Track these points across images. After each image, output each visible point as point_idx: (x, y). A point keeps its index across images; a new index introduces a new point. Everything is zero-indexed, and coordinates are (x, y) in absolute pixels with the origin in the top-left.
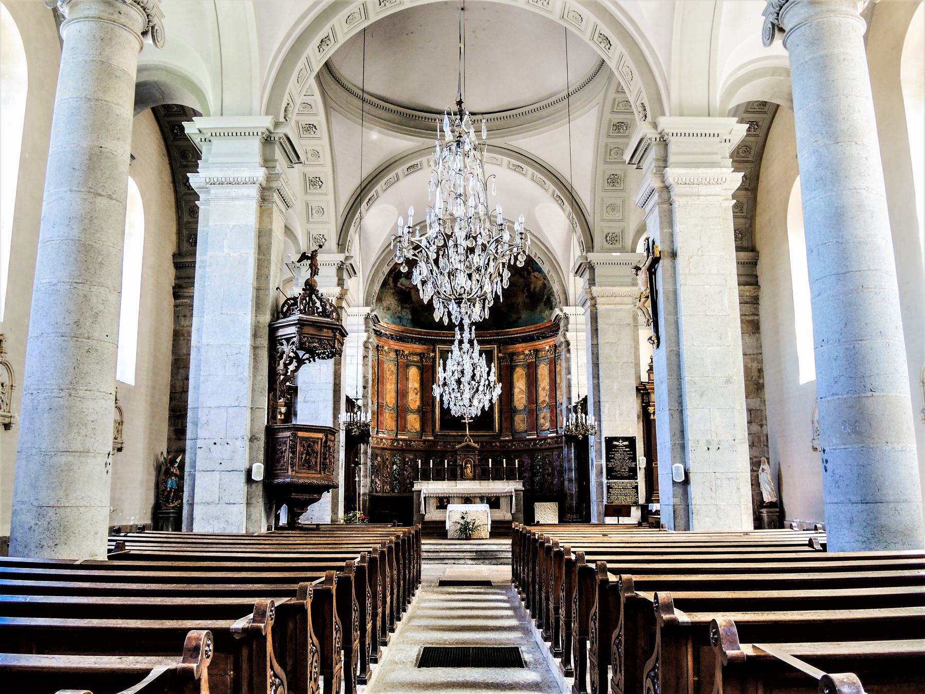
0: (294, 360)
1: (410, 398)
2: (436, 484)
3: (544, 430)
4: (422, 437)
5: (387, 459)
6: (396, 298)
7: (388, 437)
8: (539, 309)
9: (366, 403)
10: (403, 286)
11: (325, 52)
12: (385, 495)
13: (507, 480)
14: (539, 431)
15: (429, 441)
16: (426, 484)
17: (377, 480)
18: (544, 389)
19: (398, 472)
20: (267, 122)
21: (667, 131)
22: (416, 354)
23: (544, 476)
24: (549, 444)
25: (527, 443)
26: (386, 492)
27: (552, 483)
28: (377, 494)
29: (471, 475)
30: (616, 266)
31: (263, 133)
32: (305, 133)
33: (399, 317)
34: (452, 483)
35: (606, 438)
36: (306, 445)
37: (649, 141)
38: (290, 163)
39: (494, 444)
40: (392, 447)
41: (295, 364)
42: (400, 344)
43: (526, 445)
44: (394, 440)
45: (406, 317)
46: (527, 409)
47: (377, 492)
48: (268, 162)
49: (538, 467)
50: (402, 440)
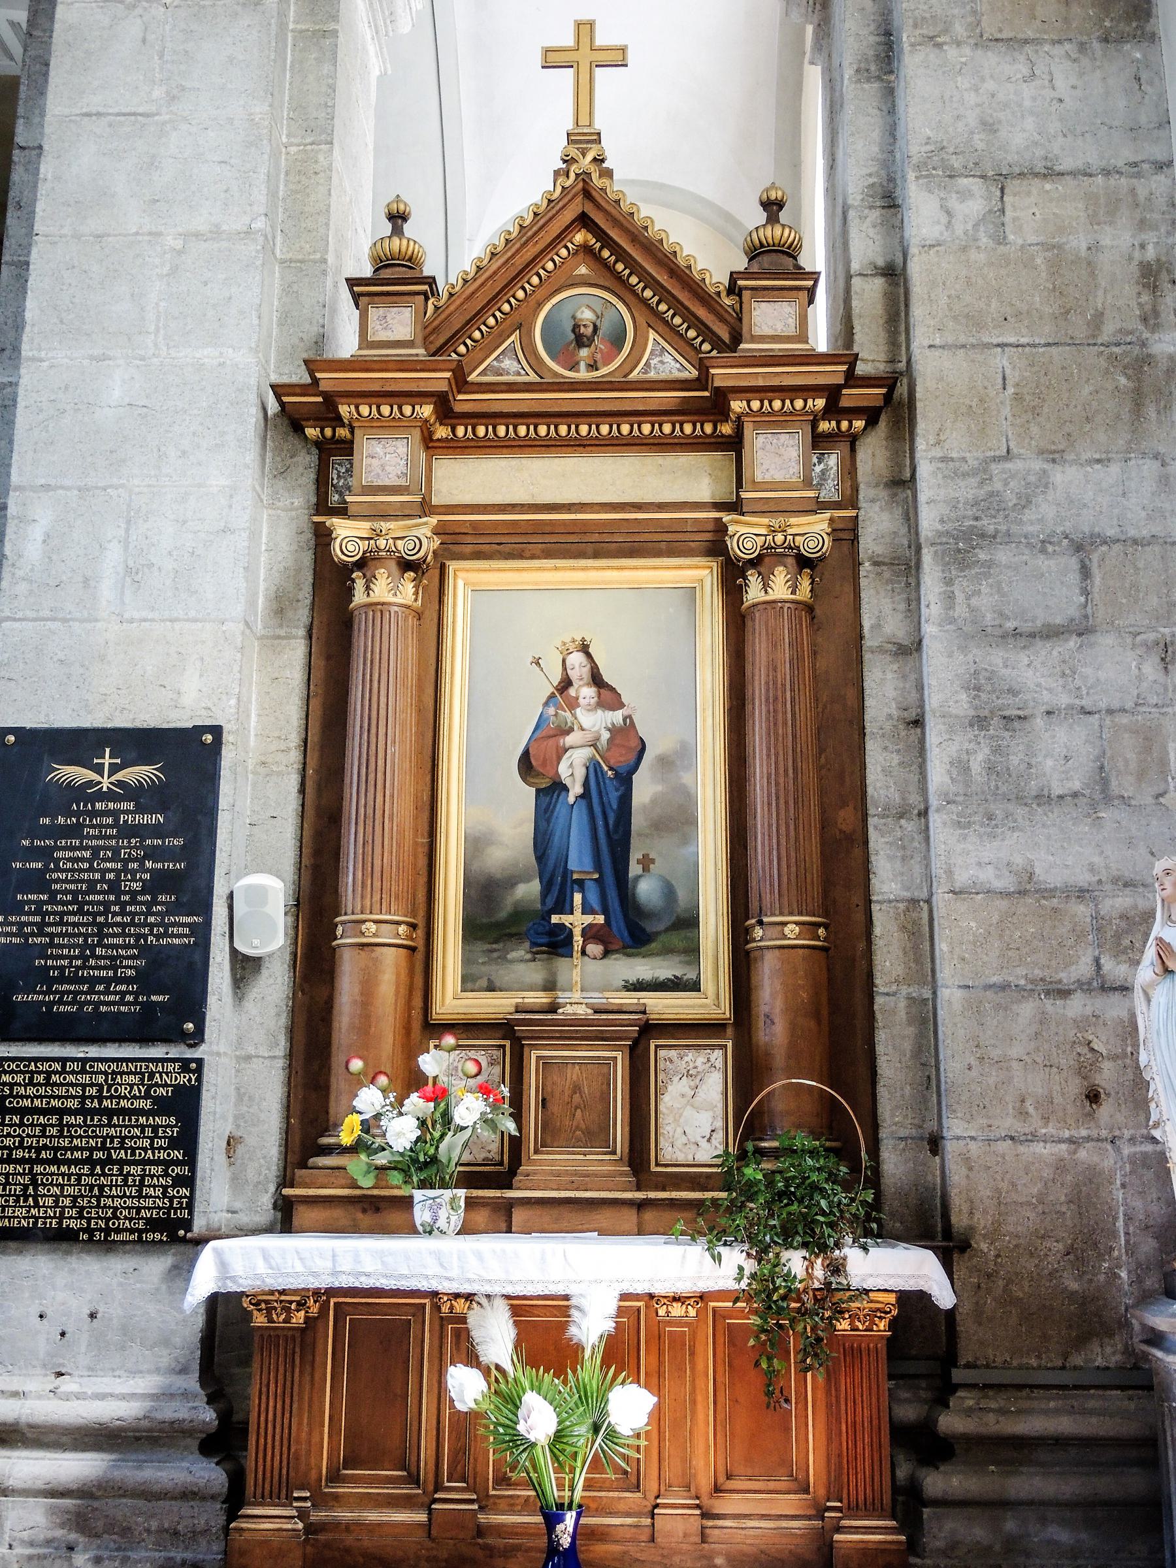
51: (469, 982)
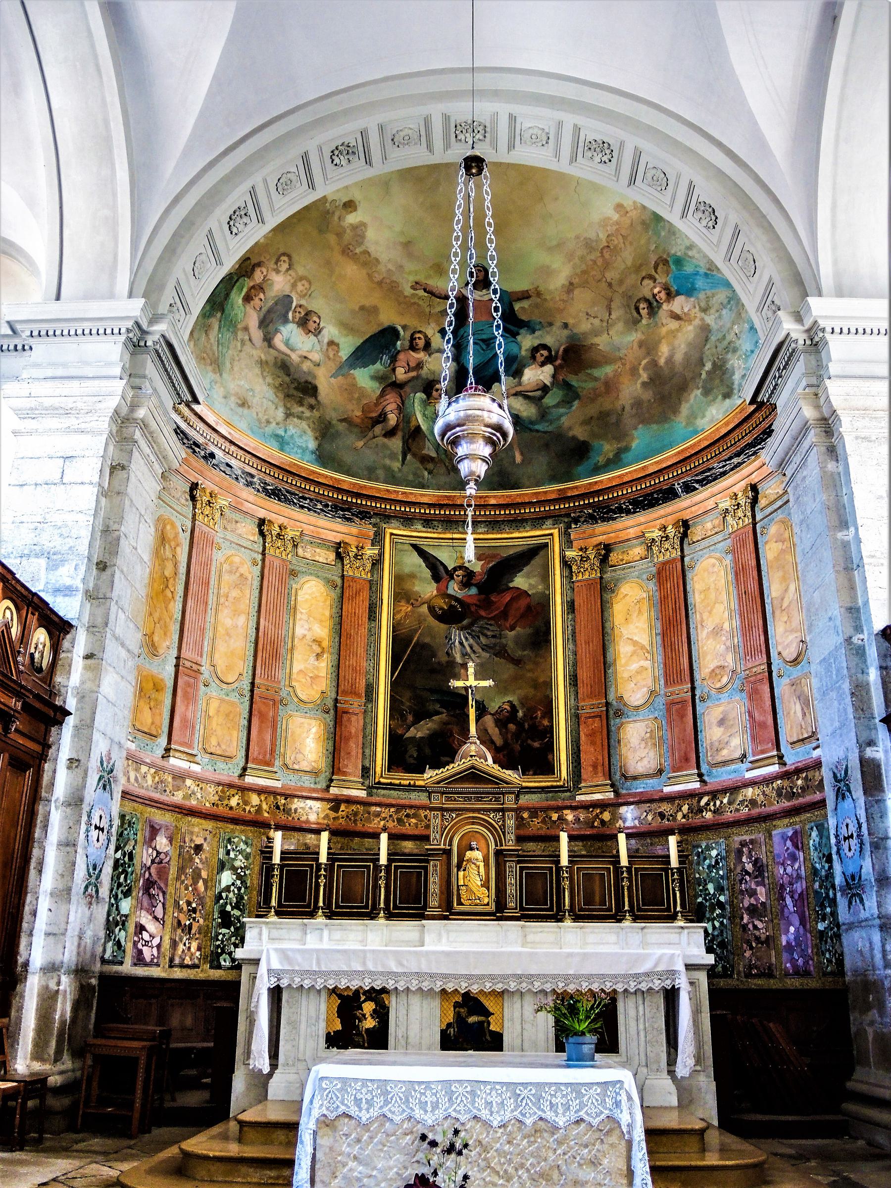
1: (297, 667)
2: (337, 935)
3: (725, 763)
4: (328, 787)
5: (198, 848)
6: (269, 379)
7: (210, 775)
8: (685, 409)
9: (99, 621)
10: (292, 350)
12: (178, 974)
13: (636, 919)
14: (704, 768)
15: (349, 801)
16: (297, 934)
17: (145, 919)
18: (717, 631)
19: (240, 897)
20: (135, 308)
21: (822, 323)
22: (323, 543)
23: (735, 916)
24: (753, 803)
25: (665, 807)
26: (182, 966)
27: (770, 942)
28: (141, 971)
29: (486, 897)
30: (874, 336)
31: (128, 331)
33: (277, 437)
34: (406, 929)
37: (793, 345)
39: (555, 817)
40: (221, 810)
42: (274, 504)
43: (662, 815)
44: (230, 786)
45: (300, 442)
46: (661, 701)
47: (139, 960)
49: (711, 888)
50: (261, 791)
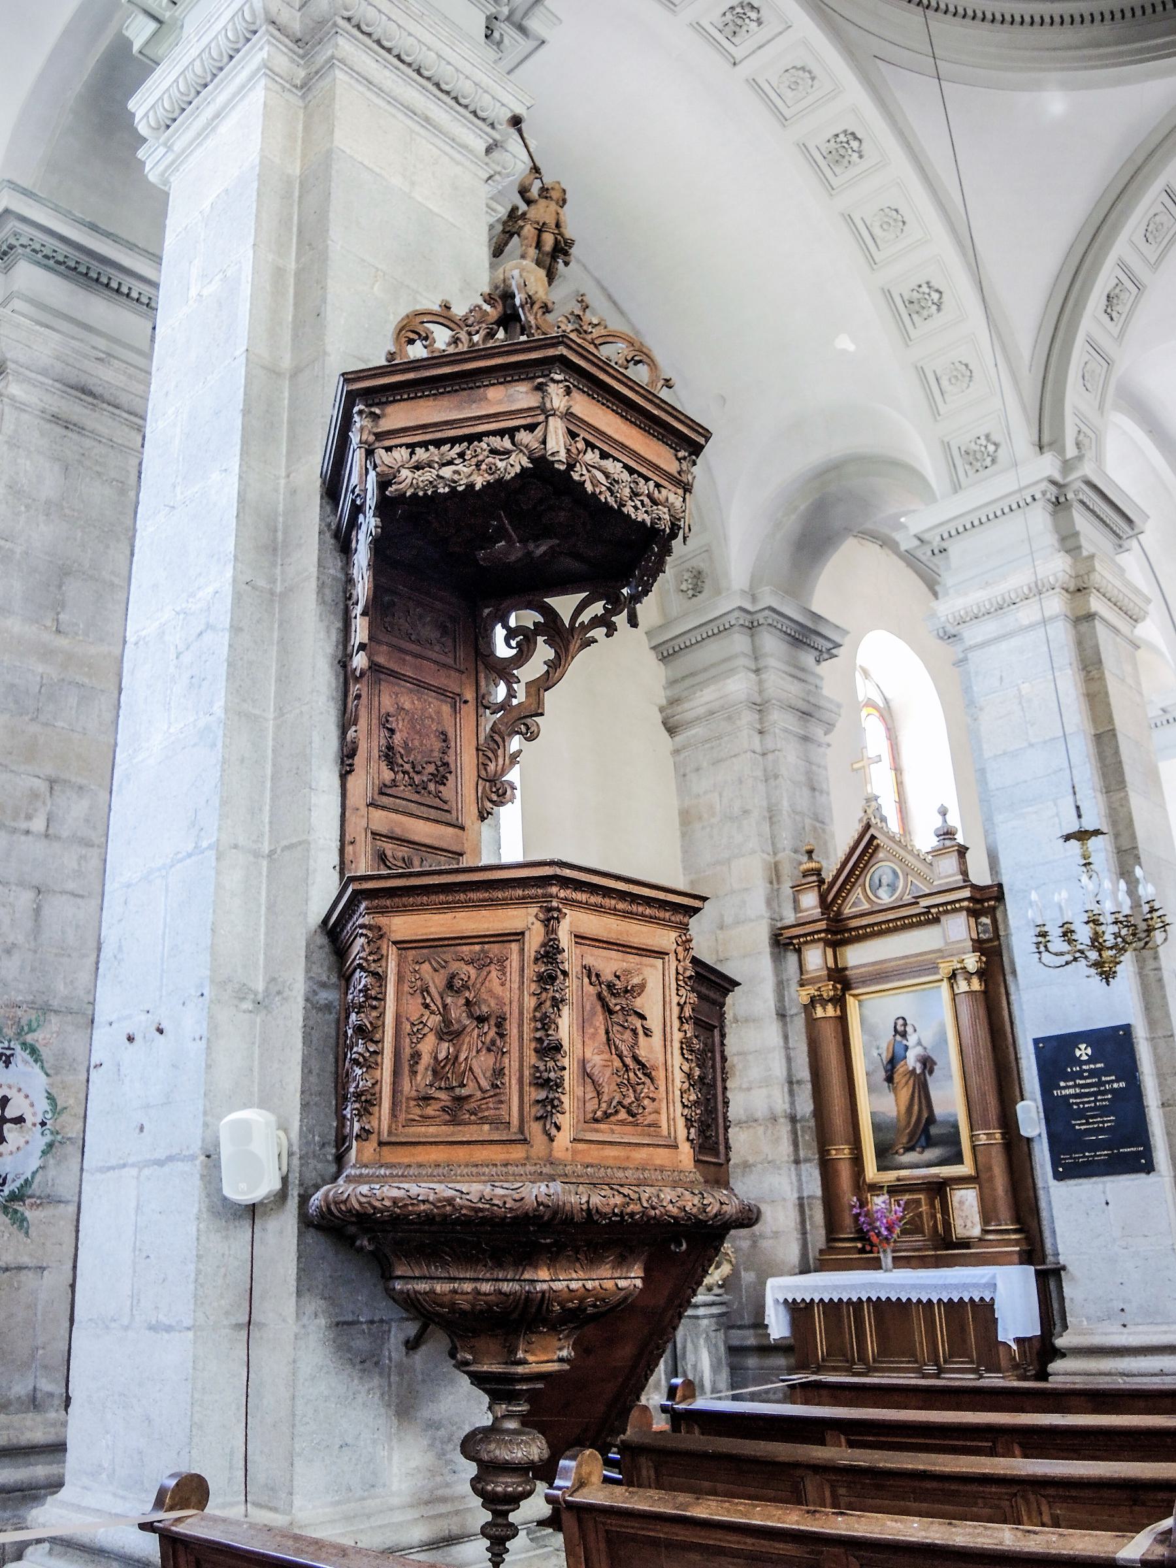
0: (540, 639)
11: (1124, 316)
32: (837, 170)
35: (1036, 1041)
36: (436, 982)
38: (1116, 541)
41: (544, 652)
48: (1069, 542)
51: (880, 1168)
